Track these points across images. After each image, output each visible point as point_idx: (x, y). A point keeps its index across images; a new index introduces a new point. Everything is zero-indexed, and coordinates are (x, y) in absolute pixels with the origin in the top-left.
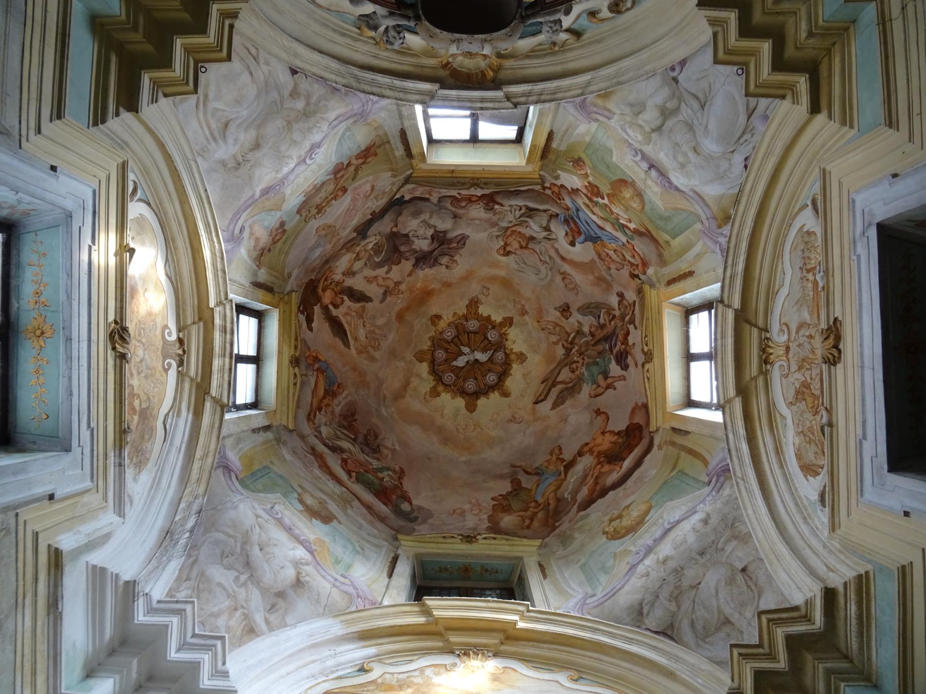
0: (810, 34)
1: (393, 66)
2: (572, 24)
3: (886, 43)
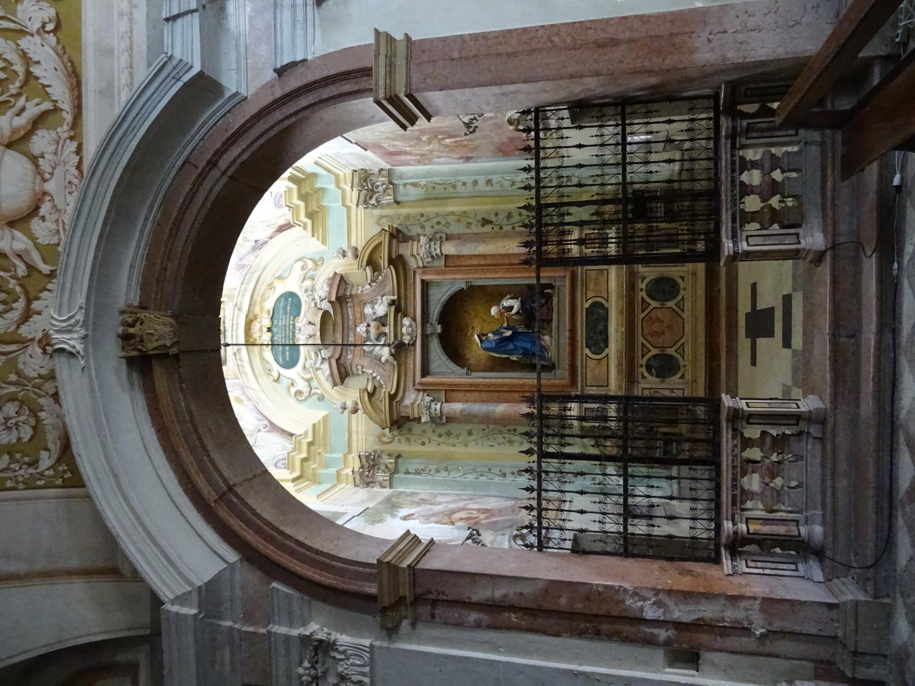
0: (314, 469)
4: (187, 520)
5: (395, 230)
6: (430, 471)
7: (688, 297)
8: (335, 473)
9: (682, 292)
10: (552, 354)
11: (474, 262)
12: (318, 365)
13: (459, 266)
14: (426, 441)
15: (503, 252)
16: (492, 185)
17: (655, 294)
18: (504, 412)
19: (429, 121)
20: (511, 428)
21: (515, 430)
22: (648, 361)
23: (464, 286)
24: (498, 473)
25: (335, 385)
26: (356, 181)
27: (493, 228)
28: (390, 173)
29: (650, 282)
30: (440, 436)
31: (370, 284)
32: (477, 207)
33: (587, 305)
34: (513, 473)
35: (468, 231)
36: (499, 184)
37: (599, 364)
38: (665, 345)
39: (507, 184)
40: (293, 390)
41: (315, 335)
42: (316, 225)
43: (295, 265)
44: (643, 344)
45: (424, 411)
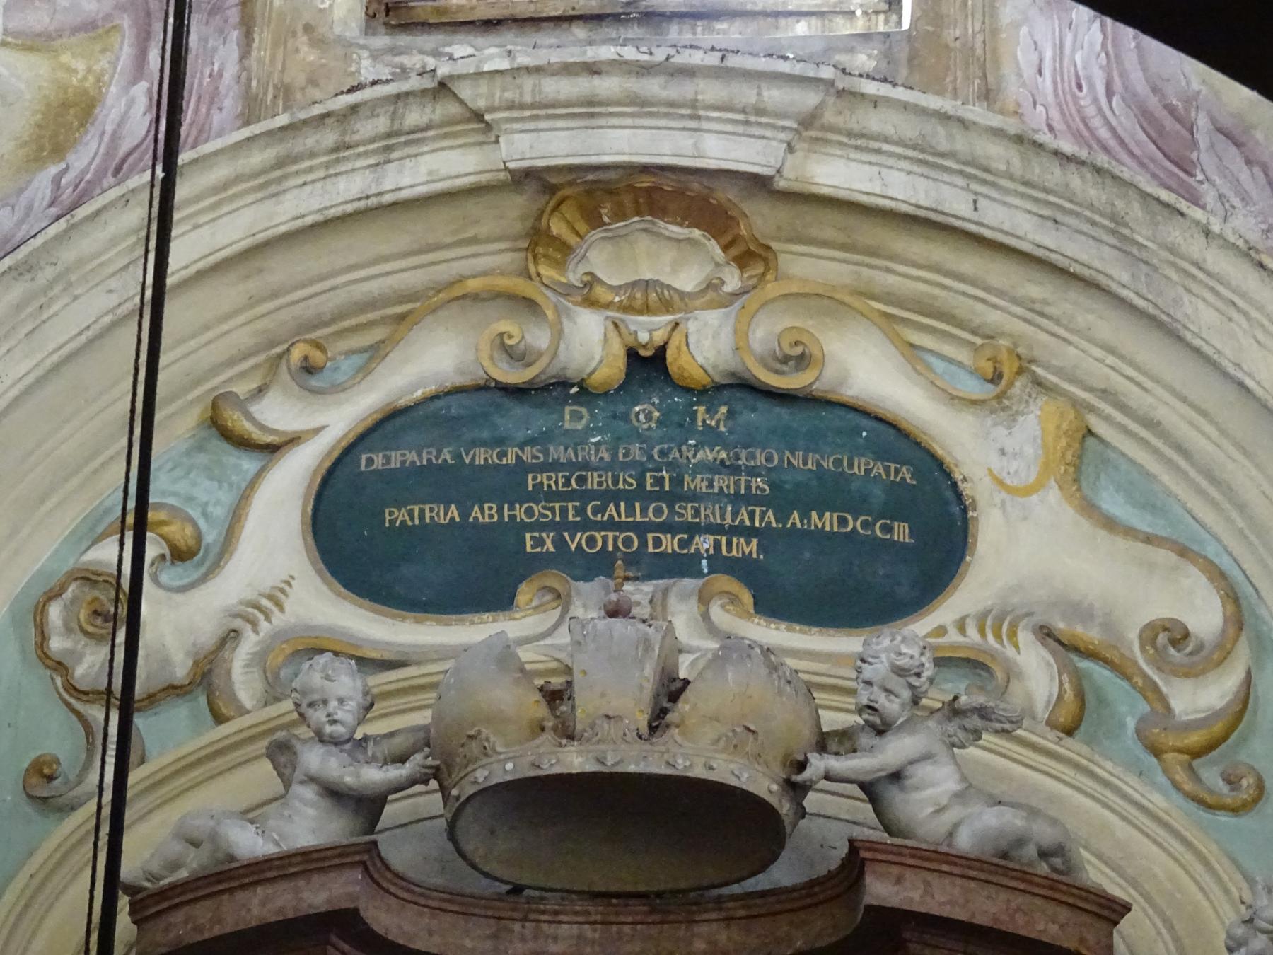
1: (970, 262)
2: (259, 475)
12: (314, 759)
19: (1126, 908)
41: (568, 733)
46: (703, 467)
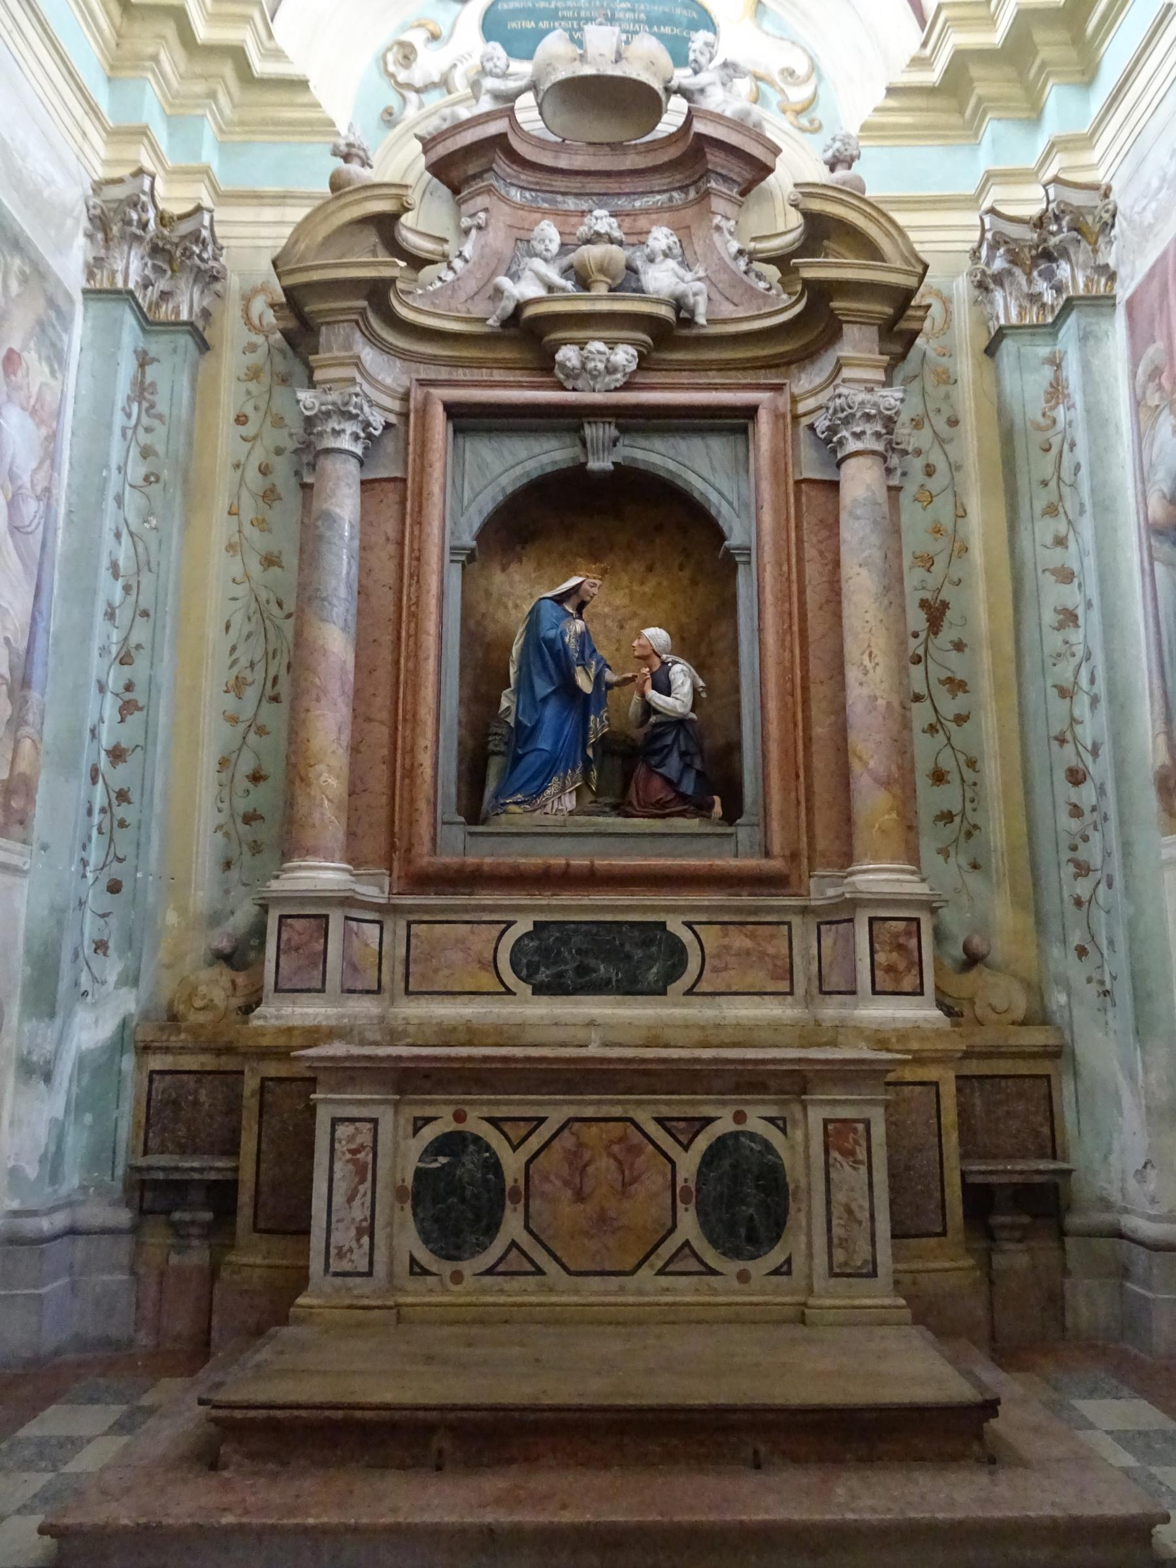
0: (155, 58)
3: (80, 89)
4: (518, 834)
5: (914, 325)
6: (148, 430)
7: (714, 1292)
8: (145, 119)
9: (732, 1267)
10: (517, 816)
11: (814, 572)
13: (798, 527)
14: (249, 430)
15: (852, 649)
16: (1061, 626)
17: (726, 1163)
18: (325, 652)
20: (284, 688)
21: (275, 699)
22: (477, 1139)
23: (735, 538)
24: (133, 642)
25: (428, 144)
26: (1077, 198)
27: (916, 635)
28: (1103, 303)
29: (768, 1147)
30: (264, 470)
31: (741, 252)
32: (981, 588)
33: (675, 925)
34: (129, 687)
35: (907, 560)
36: (1062, 648)
37: (482, 965)
38: (536, 1204)
39: (1064, 672)
40: (417, 38)
41: (582, 58)
42: (920, 102)
43: (798, 51)
44: (541, 1120)
45: (334, 397)
46: (622, 9)
